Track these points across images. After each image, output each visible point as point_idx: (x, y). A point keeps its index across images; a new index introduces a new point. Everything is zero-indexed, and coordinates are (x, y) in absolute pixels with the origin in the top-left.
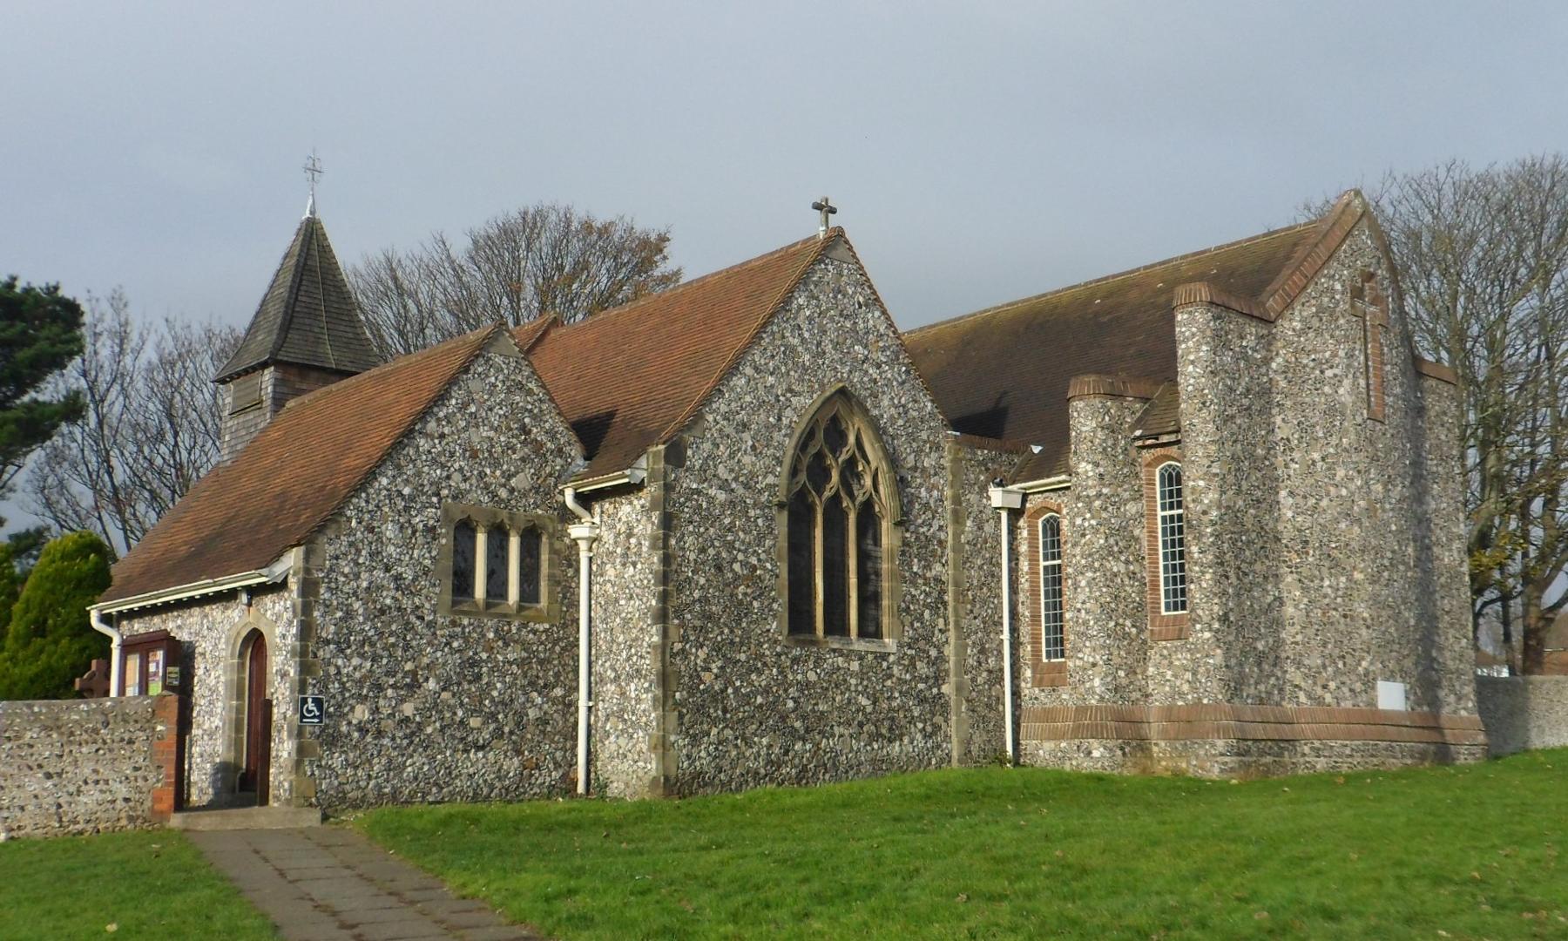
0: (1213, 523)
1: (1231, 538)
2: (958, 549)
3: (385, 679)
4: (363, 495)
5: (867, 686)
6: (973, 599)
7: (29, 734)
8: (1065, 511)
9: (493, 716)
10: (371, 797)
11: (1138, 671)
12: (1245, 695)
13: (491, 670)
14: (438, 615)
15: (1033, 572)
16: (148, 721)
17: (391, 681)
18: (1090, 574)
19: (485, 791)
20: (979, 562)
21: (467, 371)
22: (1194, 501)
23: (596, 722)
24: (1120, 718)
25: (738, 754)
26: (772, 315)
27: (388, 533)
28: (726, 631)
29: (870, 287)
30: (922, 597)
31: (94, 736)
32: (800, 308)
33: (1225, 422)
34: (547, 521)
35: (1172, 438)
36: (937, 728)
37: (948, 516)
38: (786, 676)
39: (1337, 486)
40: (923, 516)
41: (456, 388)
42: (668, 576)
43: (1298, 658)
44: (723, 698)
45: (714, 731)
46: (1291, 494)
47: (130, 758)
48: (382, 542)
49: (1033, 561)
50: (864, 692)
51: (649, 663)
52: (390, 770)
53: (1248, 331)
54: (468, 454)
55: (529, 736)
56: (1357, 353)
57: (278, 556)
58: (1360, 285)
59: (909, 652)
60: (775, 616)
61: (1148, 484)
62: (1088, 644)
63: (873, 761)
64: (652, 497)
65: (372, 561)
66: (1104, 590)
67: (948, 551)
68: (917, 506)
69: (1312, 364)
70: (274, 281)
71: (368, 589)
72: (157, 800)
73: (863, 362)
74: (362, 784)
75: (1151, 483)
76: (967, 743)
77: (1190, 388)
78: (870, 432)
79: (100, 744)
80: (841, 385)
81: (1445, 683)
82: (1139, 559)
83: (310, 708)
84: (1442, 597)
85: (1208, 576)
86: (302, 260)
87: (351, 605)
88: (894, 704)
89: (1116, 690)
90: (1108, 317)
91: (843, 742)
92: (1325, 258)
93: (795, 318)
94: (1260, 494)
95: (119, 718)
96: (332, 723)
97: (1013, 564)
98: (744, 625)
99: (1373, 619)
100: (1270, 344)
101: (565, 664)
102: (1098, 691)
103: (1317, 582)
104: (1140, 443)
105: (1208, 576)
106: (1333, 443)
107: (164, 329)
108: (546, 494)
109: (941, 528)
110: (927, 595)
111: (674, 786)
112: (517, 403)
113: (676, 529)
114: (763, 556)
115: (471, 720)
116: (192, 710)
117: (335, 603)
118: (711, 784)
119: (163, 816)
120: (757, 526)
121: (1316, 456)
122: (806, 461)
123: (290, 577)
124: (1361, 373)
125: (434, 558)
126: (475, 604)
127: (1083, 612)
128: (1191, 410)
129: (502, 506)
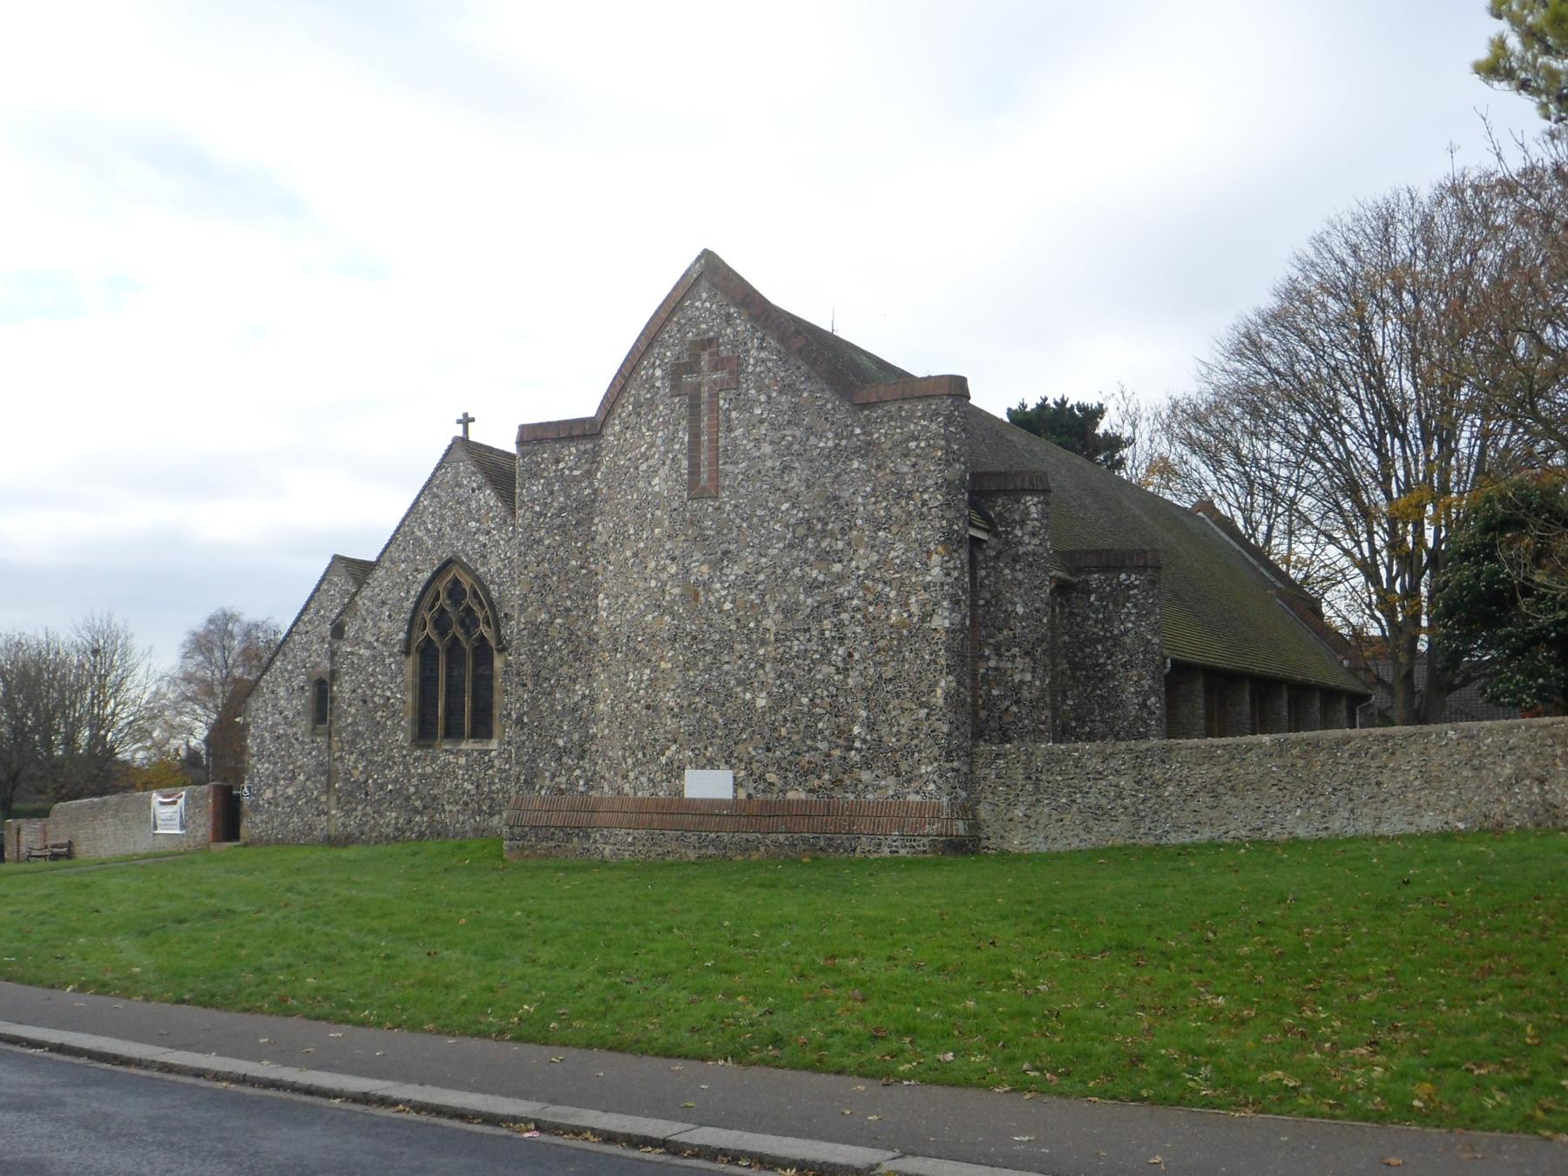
12: (537, 787)
17: (283, 776)
28: (368, 742)
39: (646, 579)
45: (360, 808)
63: (475, 830)
88: (494, 788)
103: (623, 677)
114: (395, 690)
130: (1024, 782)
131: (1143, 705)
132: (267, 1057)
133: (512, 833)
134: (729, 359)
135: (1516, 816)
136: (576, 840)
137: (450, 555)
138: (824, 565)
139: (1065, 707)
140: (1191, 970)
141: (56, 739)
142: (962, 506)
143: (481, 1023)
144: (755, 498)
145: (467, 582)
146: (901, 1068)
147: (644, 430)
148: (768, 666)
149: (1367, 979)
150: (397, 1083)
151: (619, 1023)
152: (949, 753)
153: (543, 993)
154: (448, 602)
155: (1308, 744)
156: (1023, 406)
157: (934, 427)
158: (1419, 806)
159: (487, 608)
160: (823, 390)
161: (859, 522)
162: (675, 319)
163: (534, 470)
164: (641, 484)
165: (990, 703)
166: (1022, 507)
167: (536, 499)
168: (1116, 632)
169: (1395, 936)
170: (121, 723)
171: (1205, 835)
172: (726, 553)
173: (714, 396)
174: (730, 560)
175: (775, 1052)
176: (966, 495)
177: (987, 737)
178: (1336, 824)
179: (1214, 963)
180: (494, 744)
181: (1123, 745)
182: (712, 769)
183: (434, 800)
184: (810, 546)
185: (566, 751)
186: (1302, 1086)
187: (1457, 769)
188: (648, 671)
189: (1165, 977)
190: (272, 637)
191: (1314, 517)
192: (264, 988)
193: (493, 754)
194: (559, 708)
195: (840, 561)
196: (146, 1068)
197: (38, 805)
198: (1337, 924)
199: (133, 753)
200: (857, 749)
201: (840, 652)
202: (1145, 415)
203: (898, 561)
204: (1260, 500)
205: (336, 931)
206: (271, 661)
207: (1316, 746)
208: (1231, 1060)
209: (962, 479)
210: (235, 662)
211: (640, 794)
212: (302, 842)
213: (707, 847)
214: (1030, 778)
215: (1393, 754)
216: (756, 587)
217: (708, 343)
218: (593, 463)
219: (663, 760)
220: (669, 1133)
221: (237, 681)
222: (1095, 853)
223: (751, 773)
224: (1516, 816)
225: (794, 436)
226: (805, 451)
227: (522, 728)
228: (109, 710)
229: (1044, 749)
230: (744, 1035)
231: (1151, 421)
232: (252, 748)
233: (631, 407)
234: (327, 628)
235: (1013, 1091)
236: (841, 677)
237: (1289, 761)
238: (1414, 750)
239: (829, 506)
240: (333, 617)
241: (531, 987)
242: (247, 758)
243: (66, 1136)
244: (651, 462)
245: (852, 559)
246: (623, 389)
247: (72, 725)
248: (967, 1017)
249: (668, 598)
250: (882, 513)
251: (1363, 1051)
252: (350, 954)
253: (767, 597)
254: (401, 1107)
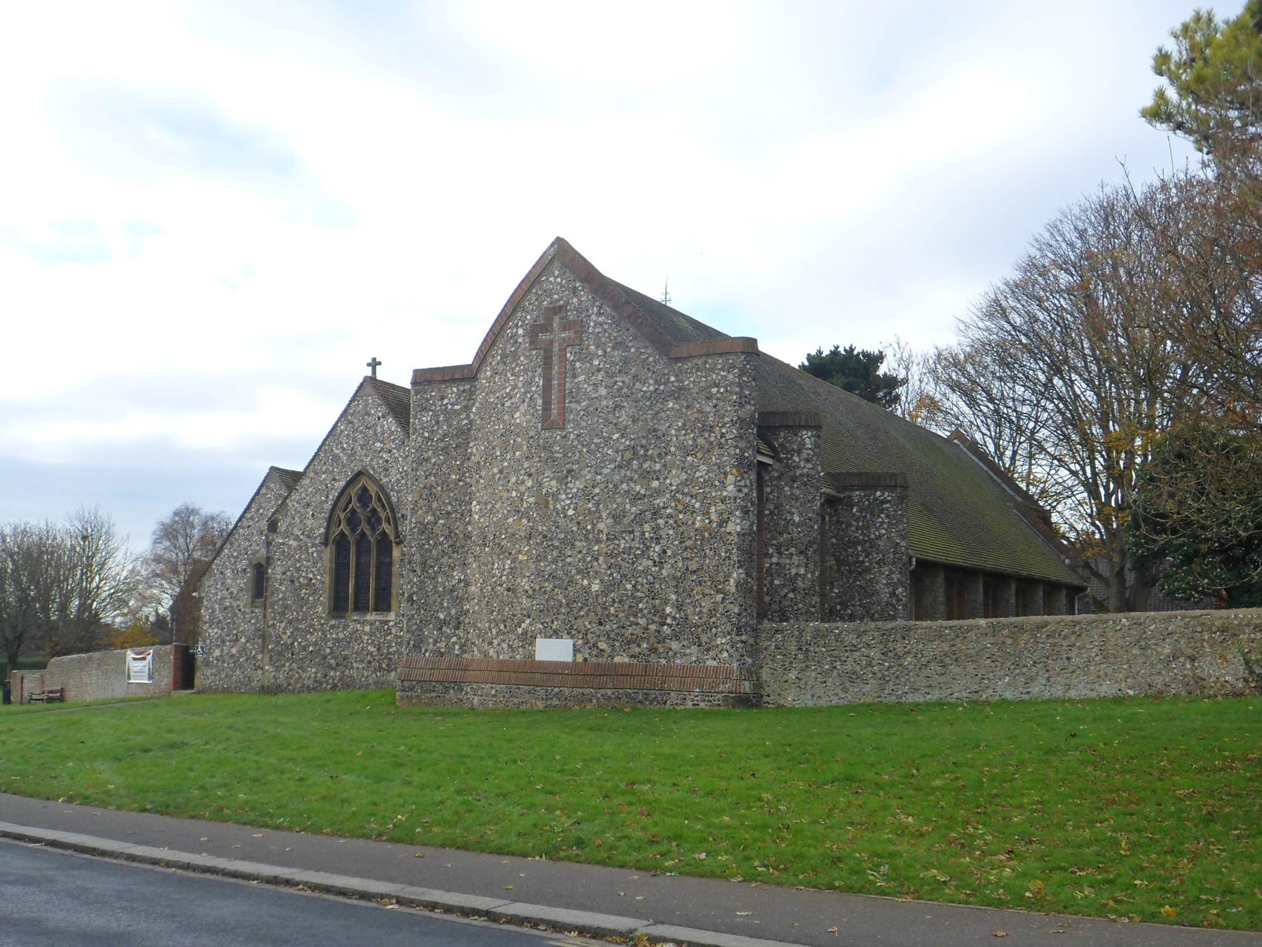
12: (423, 650)
17: (228, 639)
28: (295, 613)
45: (287, 664)
63: (376, 683)
88: (391, 650)
103: (490, 566)
114: (316, 573)
130: (796, 653)
131: (893, 594)
132: (205, 851)
133: (403, 686)
134: (575, 322)
135: (1173, 686)
136: (452, 692)
137: (360, 468)
138: (645, 481)
139: (832, 594)
140: (894, 797)
141: (54, 607)
142: (751, 438)
143: (365, 828)
144: (593, 429)
145: (373, 490)
146: (666, 864)
147: (509, 375)
148: (601, 559)
149: (1021, 806)
150: (299, 870)
151: (466, 829)
152: (739, 629)
153: (413, 807)
154: (358, 505)
155: (1016, 627)
156: (820, 352)
157: (731, 376)
158: (1099, 677)
159: (388, 510)
160: (646, 347)
161: (673, 449)
162: (534, 291)
163: (424, 405)
164: (506, 417)
165: (773, 591)
166: (799, 439)
167: (425, 427)
168: (872, 536)
169: (1052, 775)
170: (104, 595)
171: (934, 696)
172: (570, 471)
173: (563, 350)
174: (573, 477)
175: (578, 852)
176: (755, 430)
177: (770, 617)
178: (1035, 689)
179: (912, 792)
180: (392, 616)
181: (873, 625)
182: (557, 638)
183: (344, 659)
184: (635, 467)
185: (445, 622)
186: (949, 881)
187: (1128, 648)
188: (509, 562)
189: (873, 802)
190: (224, 527)
191: (1047, 445)
192: (206, 800)
193: (391, 623)
194: (441, 589)
195: (658, 479)
196: (116, 858)
197: (37, 659)
198: (1011, 765)
199: (113, 618)
200: (668, 625)
201: (656, 550)
202: (916, 361)
203: (702, 480)
204: (1007, 431)
205: (263, 759)
206: (221, 548)
207: (1021, 628)
208: (905, 862)
209: (752, 416)
210: (195, 546)
211: (501, 657)
212: (242, 691)
213: (552, 699)
214: (801, 649)
215: (1080, 635)
216: (593, 498)
217: (558, 310)
218: (470, 400)
219: (520, 631)
220: (491, 906)
221: (196, 562)
222: (844, 710)
223: (586, 641)
224: (1173, 686)
225: (623, 382)
226: (632, 393)
227: (412, 605)
228: (94, 584)
229: (813, 627)
230: (556, 838)
231: (921, 365)
232: (205, 616)
233: (499, 357)
234: (264, 524)
235: (744, 881)
236: (657, 569)
237: (1000, 640)
238: (1095, 634)
239: (650, 436)
240: (270, 515)
241: (405, 802)
242: (201, 624)
243: (57, 902)
244: (513, 400)
245: (667, 477)
246: (494, 343)
247: (65, 595)
248: (722, 828)
249: (525, 505)
250: (690, 442)
251: (1003, 857)
252: (273, 777)
253: (601, 506)
254: (301, 887)
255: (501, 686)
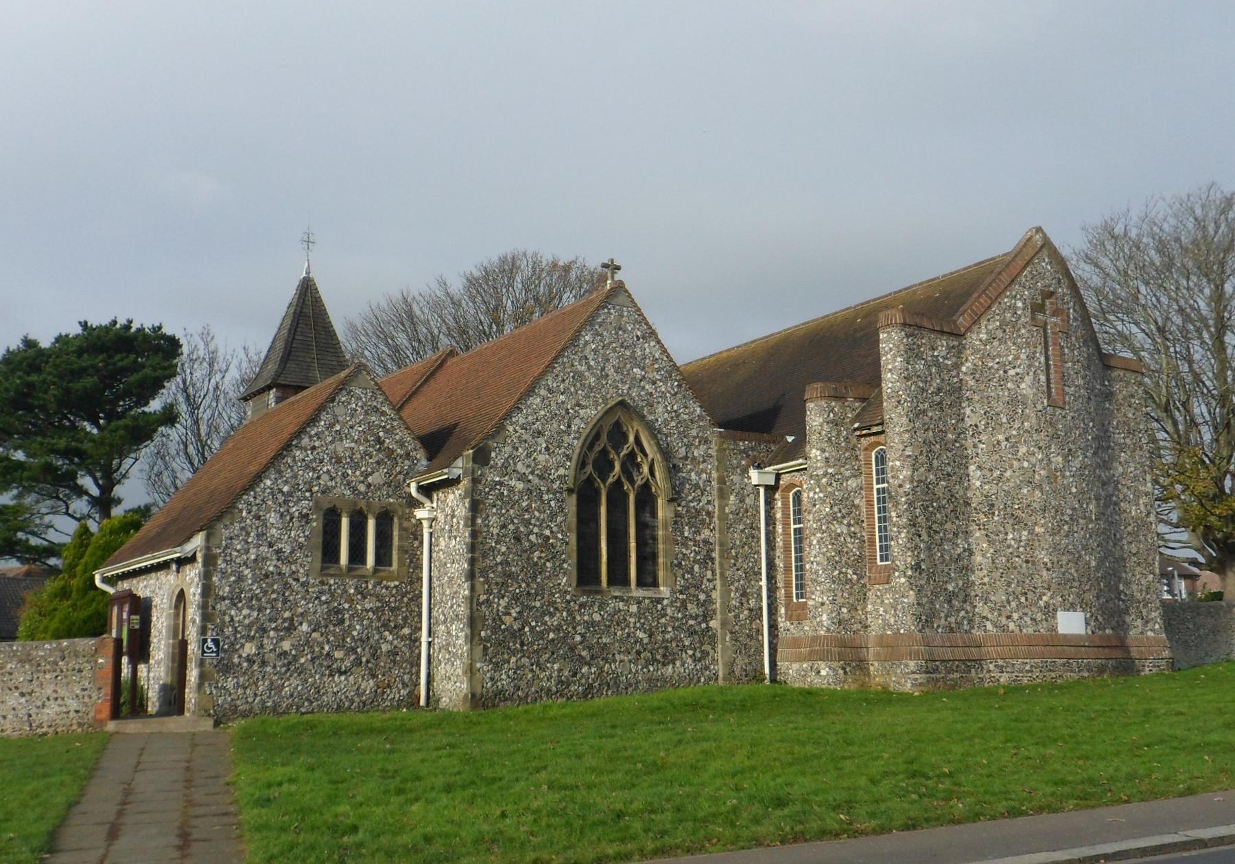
0: (907, 494)
1: (922, 505)
2: (723, 516)
3: (268, 624)
4: (252, 493)
5: (644, 624)
6: (736, 556)
7: (9, 666)
8: (805, 487)
9: (354, 650)
10: (257, 709)
11: (859, 608)
12: (935, 626)
13: (352, 616)
14: (310, 578)
15: (786, 533)
16: (92, 656)
17: (273, 626)
18: (819, 535)
19: (347, 704)
20: (741, 527)
21: (333, 400)
22: (893, 477)
23: (434, 653)
24: (842, 644)
25: (534, 676)
26: (563, 350)
27: (271, 520)
28: (524, 585)
29: (647, 324)
30: (692, 555)
31: (55, 666)
32: (587, 343)
33: (917, 416)
34: (398, 507)
35: (879, 429)
36: (705, 654)
37: (715, 493)
38: (574, 618)
39: (1019, 460)
40: (693, 494)
41: (325, 413)
42: (476, 546)
43: (985, 596)
44: (521, 635)
45: (513, 659)
46: (979, 467)
47: (79, 682)
48: (266, 526)
49: (786, 525)
50: (642, 628)
51: (463, 610)
52: (272, 690)
53: (940, 343)
54: (333, 460)
55: (382, 664)
56: (1038, 355)
57: (188, 538)
58: (1040, 302)
59: (681, 597)
60: (565, 574)
61: (865, 464)
62: (818, 588)
63: (649, 680)
64: (465, 488)
65: (258, 540)
66: (830, 547)
67: (715, 519)
68: (687, 486)
69: (996, 366)
70: (281, 325)
71: (256, 560)
72: (99, 711)
73: (641, 380)
74: (250, 700)
75: (869, 464)
76: (730, 666)
77: (889, 390)
78: (647, 433)
79: (58, 672)
80: (620, 399)
81: (1132, 610)
82: (859, 522)
83: (210, 646)
84: (1130, 543)
85: (903, 535)
86: (299, 309)
87: (242, 572)
88: (668, 636)
89: (840, 623)
90: (862, 333)
91: (623, 666)
92: (1007, 283)
93: (582, 351)
94: (950, 469)
95: (72, 654)
96: (227, 656)
97: (771, 528)
98: (539, 580)
99: (1053, 563)
100: (960, 352)
101: (412, 611)
102: (825, 624)
104: (858, 433)
105: (903, 535)
106: (1016, 426)
107: (242, 355)
108: (397, 487)
109: (709, 502)
110: (697, 553)
111: (477, 700)
112: (374, 422)
113: (482, 511)
114: (555, 529)
115: (336, 653)
116: (150, 646)
117: (229, 570)
118: (511, 698)
119: (101, 723)
120: (550, 506)
121: (1001, 437)
122: (592, 457)
123: (198, 553)
124: (1042, 371)
125: (307, 536)
126: (340, 569)
127: (815, 564)
128: (890, 407)
129: (361, 497)
219: (1042, 603)
255: (1036, 660)
